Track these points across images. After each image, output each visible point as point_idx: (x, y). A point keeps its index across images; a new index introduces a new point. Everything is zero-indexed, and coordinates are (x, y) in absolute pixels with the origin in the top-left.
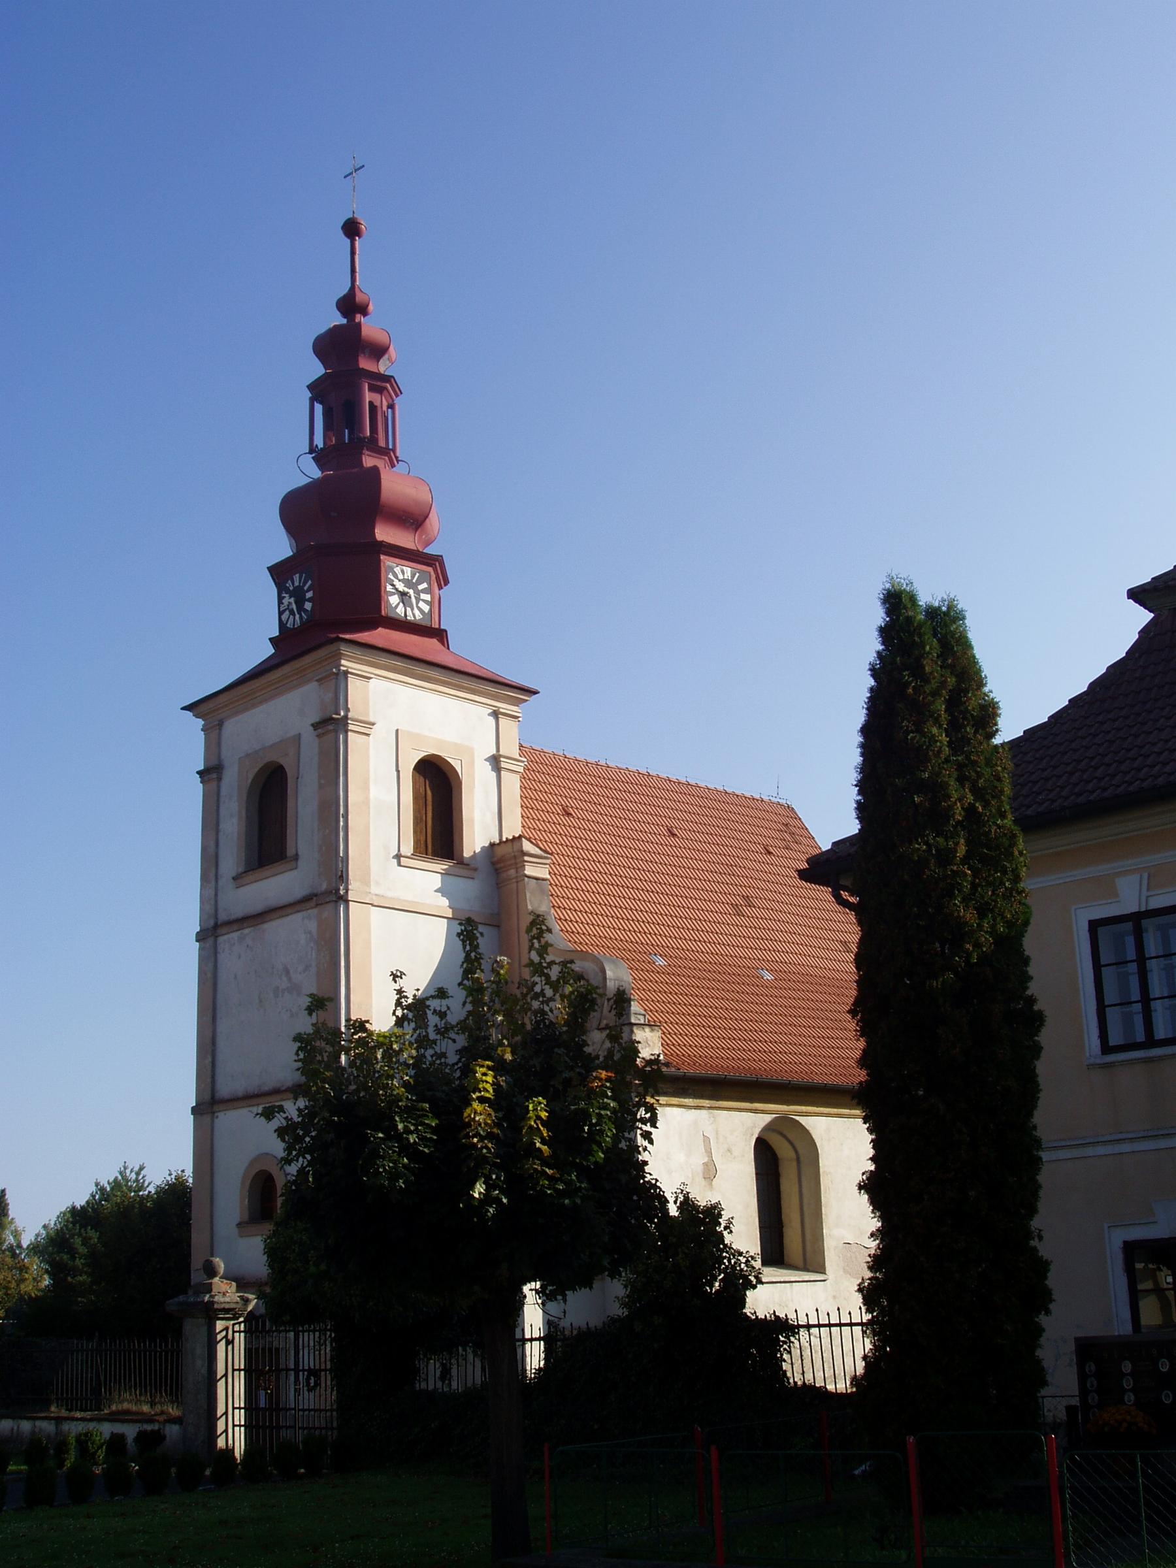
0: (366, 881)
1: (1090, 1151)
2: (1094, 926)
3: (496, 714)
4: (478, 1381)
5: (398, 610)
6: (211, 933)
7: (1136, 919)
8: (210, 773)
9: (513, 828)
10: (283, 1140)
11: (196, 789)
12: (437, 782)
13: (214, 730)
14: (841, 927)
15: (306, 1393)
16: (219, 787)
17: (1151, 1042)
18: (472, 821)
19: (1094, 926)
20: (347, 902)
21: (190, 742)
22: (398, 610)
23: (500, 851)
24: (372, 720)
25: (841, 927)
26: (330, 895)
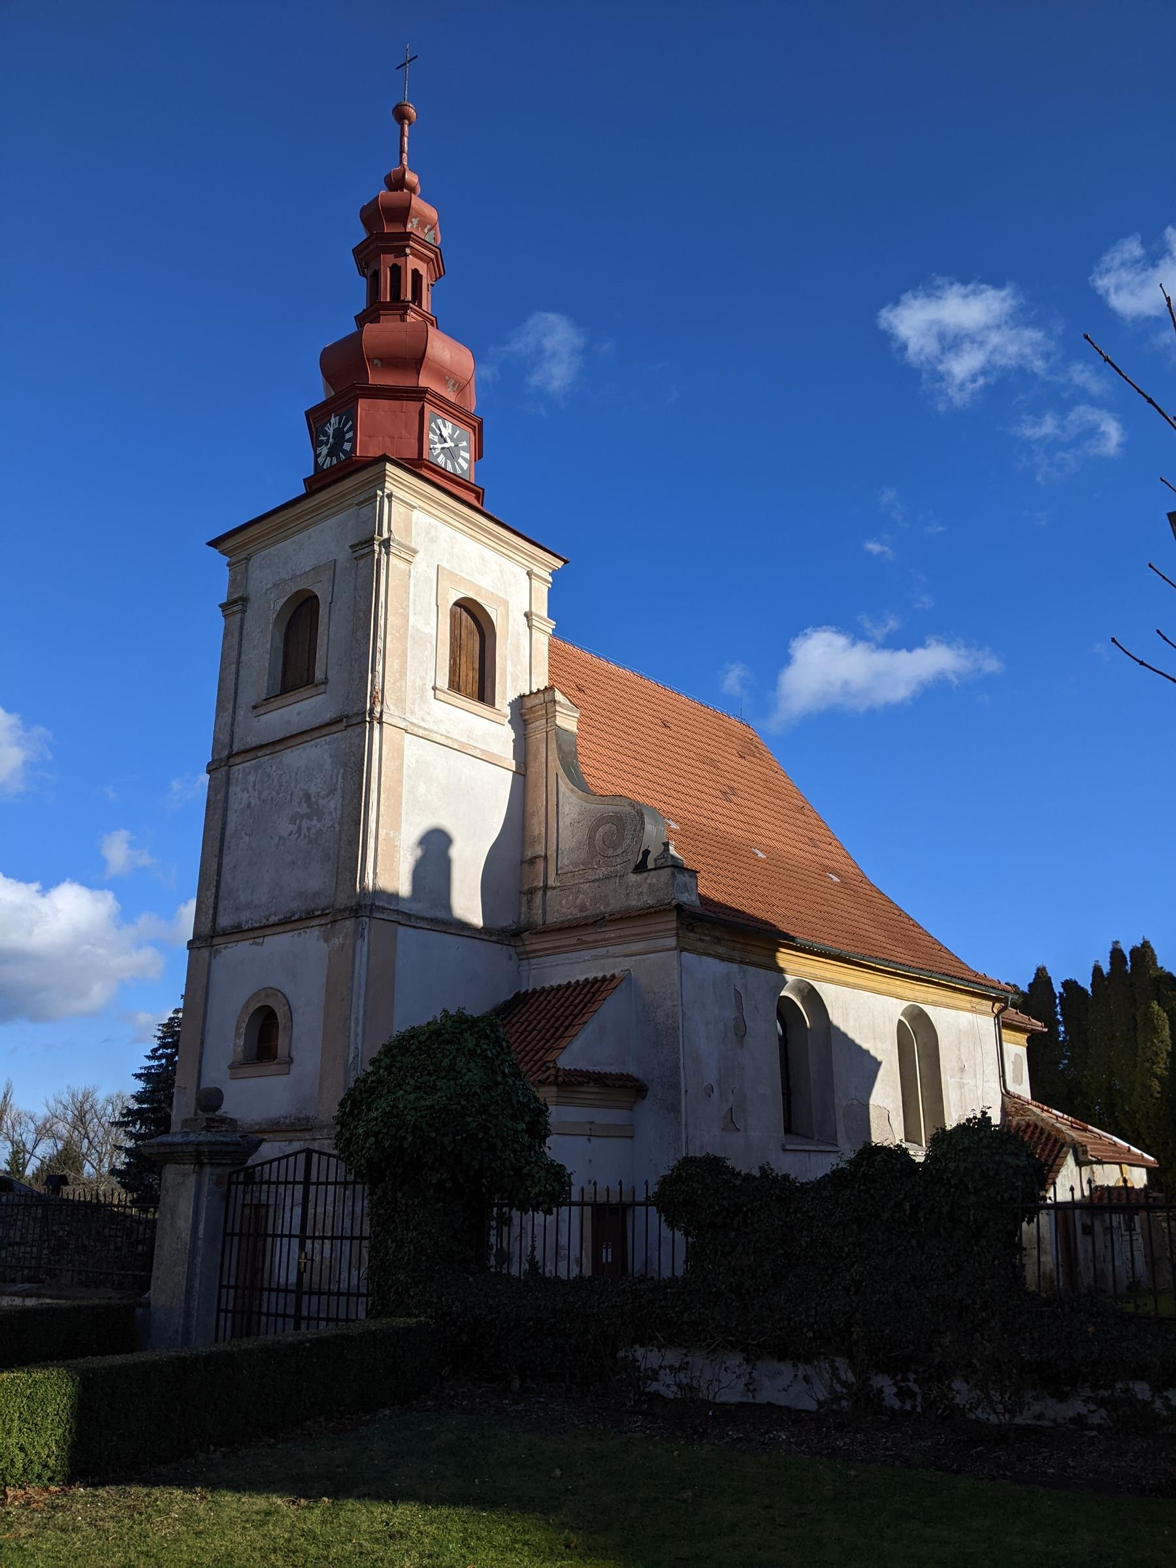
0: (401, 702)
3: (529, 574)
4: (679, 1273)
5: (439, 460)
6: (224, 763)
8: (236, 606)
9: (541, 681)
10: (364, 275)
11: (218, 623)
12: (473, 625)
13: (239, 565)
15: (272, 1201)
16: (242, 621)
18: (504, 669)
20: (381, 723)
21: (215, 576)
22: (439, 460)
23: (529, 703)
24: (413, 545)
26: (355, 719)
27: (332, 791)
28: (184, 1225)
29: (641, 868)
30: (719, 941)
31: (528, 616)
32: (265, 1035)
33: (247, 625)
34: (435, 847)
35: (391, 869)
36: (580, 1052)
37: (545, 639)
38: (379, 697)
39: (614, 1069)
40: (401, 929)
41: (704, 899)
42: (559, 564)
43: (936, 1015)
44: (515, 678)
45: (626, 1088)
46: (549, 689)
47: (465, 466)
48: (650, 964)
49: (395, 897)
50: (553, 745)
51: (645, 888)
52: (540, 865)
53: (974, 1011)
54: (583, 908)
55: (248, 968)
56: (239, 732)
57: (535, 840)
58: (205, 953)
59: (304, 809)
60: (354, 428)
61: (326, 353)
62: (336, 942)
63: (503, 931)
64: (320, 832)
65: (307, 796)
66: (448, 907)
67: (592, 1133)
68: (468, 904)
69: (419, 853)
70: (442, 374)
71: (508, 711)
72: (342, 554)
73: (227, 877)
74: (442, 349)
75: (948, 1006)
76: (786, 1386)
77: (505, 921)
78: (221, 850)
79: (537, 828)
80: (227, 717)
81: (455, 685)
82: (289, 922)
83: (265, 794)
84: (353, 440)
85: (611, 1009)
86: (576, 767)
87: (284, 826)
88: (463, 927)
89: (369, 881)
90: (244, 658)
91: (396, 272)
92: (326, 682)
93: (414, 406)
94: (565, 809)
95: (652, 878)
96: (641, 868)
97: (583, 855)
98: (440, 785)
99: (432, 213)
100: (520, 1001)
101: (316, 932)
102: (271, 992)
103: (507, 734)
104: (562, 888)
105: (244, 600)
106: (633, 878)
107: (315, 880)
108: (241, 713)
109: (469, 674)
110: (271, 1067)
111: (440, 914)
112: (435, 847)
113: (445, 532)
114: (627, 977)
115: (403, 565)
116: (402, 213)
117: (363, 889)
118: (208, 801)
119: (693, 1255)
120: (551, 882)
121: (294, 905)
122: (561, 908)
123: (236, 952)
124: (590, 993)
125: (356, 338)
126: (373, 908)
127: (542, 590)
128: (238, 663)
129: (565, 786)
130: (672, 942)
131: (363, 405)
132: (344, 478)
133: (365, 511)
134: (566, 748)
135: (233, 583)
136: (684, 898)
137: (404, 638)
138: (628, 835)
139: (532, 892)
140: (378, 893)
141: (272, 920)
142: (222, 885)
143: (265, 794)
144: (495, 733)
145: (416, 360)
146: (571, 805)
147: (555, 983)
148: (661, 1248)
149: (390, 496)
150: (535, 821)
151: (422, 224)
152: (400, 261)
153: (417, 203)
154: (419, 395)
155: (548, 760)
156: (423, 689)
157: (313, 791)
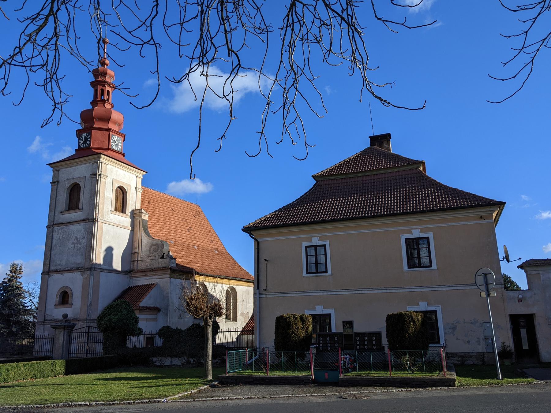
0: (102, 216)
1: (303, 294)
2: (307, 247)
3: (137, 177)
6: (52, 226)
7: (316, 247)
8: (55, 183)
9: (138, 207)
12: (122, 192)
14: (154, 233)
16: (57, 188)
17: (317, 272)
19: (307, 247)
25: (154, 233)
26: (90, 220)
27: (84, 238)
28: (61, 341)
29: (162, 257)
30: (180, 275)
31: (136, 188)
32: (65, 298)
33: (58, 189)
34: (109, 251)
35: (98, 258)
36: (145, 302)
37: (140, 194)
38: (97, 215)
39: (153, 306)
40: (101, 273)
41: (177, 264)
42: (145, 173)
43: (237, 288)
44: (132, 205)
45: (156, 310)
46: (141, 209)
47: (120, 147)
48: (162, 280)
49: (100, 265)
50: (141, 224)
51: (163, 263)
52: (137, 255)
53: (248, 286)
54: (147, 266)
55: (59, 282)
56: (56, 219)
57: (135, 248)
58: (47, 276)
59: (76, 241)
60: (90, 138)
61: (82, 113)
62: (85, 276)
63: (126, 271)
64: (80, 248)
65: (77, 238)
66: (112, 266)
67: (147, 320)
68: (117, 265)
69: (105, 253)
70: (115, 123)
71: (129, 214)
72: (88, 175)
73: (53, 257)
74: (116, 115)
75: (240, 285)
76: (177, 361)
77: (127, 269)
78: (51, 249)
79: (136, 245)
80: (52, 213)
81: (116, 210)
82: (71, 270)
83: (64, 236)
84: (90, 141)
85: (153, 292)
86: (147, 229)
87: (70, 245)
88: (116, 271)
89: (94, 261)
90: (57, 198)
91: (102, 91)
92: (82, 209)
93: (107, 133)
94: (144, 241)
95: (165, 260)
96: (162, 257)
97: (148, 253)
98: (112, 235)
99: (113, 73)
100: (130, 288)
101: (79, 273)
102: (68, 287)
103: (129, 220)
104: (142, 261)
105: (58, 182)
106: (160, 260)
107: (79, 260)
108: (57, 213)
109: (120, 207)
110: (66, 306)
111: (110, 268)
112: (109, 251)
113: (115, 169)
114: (157, 284)
115: (104, 180)
116: (104, 74)
117: (92, 263)
118: (47, 236)
119: (164, 342)
120: (139, 259)
121: (73, 266)
122: (142, 266)
123: (56, 277)
124: (149, 287)
125: (92, 110)
126: (95, 268)
127: (140, 181)
128: (56, 199)
129: (144, 235)
130: (169, 276)
131: (93, 132)
132: (88, 152)
133: (94, 165)
134: (145, 224)
135: (54, 176)
136: (173, 265)
137: (104, 199)
138: (160, 249)
139: (134, 261)
140: (96, 264)
141: (67, 269)
142: (51, 259)
143: (64, 236)
144: (126, 220)
145: (107, 119)
146: (145, 240)
147: (139, 284)
148: (159, 342)
149: (101, 162)
150: (135, 243)
151: (110, 77)
152: (104, 88)
153: (109, 71)
154: (109, 130)
155: (139, 227)
156: (108, 211)
157: (78, 237)
